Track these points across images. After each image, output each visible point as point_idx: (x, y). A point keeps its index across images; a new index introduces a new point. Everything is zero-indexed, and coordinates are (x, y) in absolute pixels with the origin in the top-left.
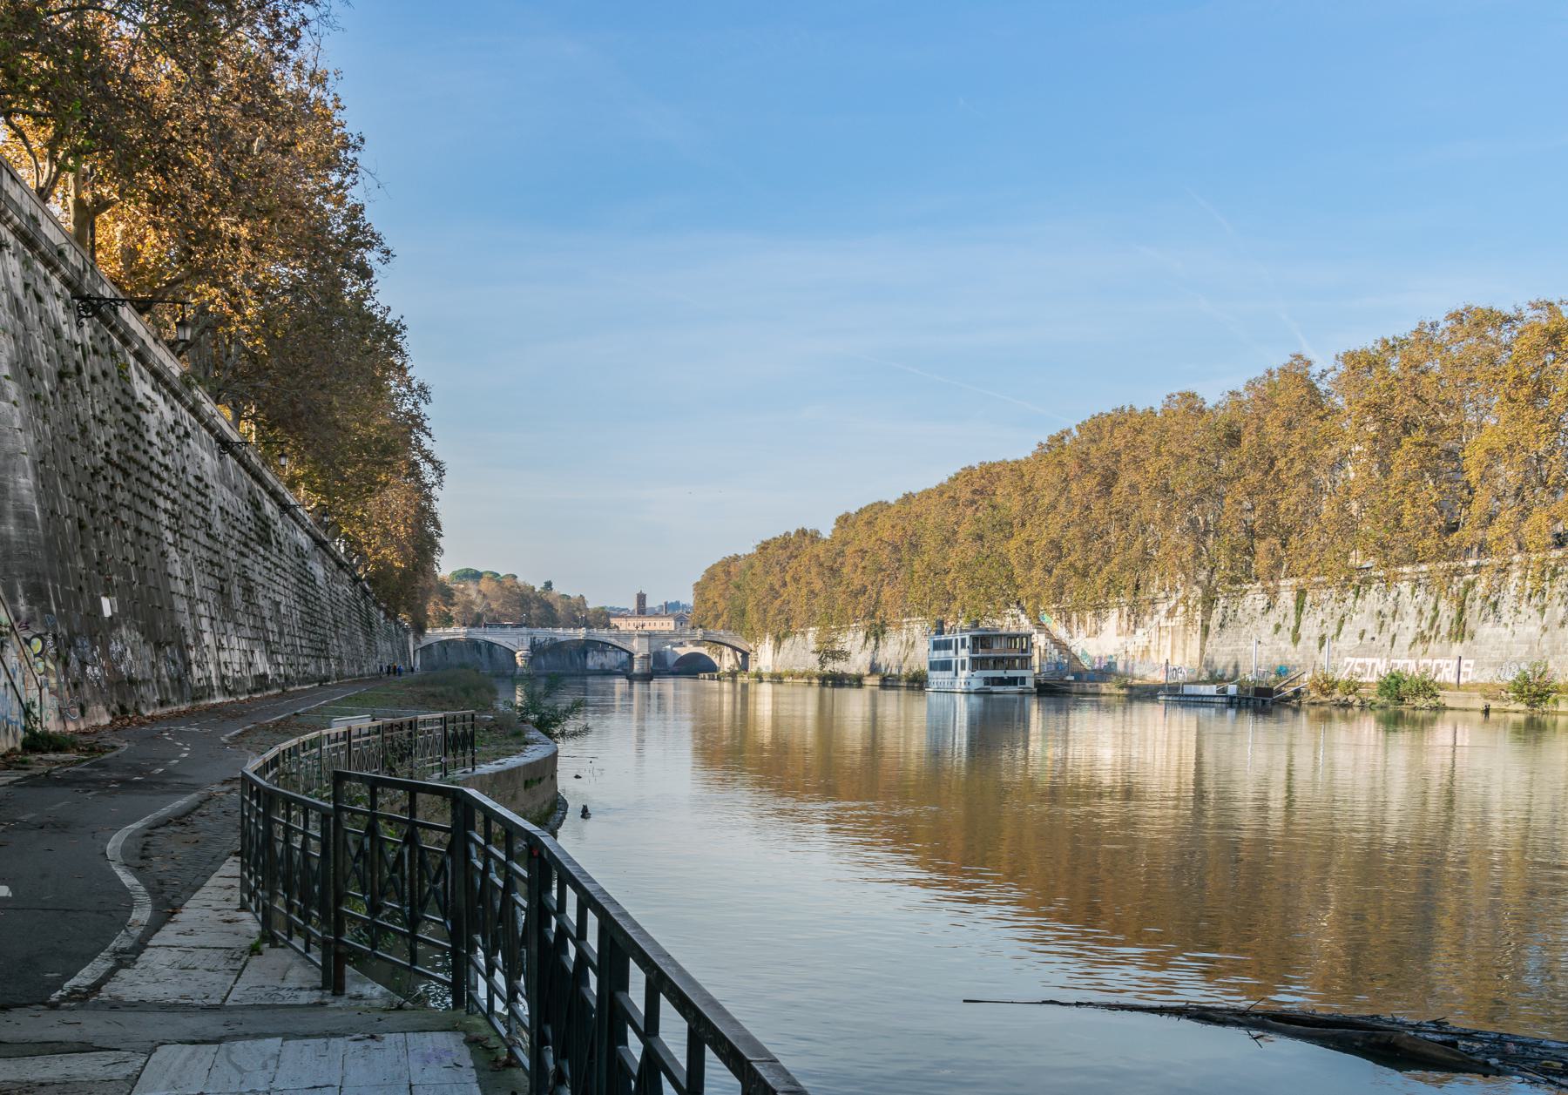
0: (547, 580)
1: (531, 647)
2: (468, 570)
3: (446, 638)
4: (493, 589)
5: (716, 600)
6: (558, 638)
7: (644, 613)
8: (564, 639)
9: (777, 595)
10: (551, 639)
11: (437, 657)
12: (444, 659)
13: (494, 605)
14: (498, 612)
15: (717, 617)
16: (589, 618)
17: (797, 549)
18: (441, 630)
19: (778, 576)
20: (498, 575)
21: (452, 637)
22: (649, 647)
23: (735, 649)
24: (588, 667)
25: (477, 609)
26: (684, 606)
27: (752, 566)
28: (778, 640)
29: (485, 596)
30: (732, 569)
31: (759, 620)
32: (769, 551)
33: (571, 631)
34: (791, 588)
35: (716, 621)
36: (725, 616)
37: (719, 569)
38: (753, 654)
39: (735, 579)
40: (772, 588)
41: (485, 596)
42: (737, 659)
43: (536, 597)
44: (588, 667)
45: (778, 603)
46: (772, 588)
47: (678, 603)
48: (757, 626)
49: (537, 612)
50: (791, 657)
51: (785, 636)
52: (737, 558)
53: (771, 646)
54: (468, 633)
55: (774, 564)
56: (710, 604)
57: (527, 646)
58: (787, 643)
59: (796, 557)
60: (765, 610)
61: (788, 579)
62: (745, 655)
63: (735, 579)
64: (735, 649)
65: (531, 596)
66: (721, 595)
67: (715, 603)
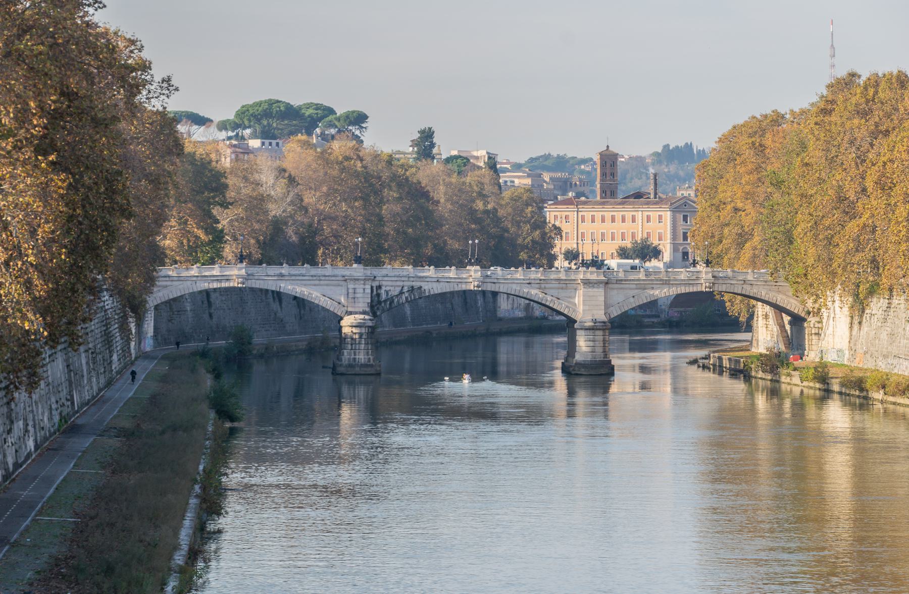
0: (424, 126)
1: (371, 306)
2: (271, 103)
3: (205, 286)
4: (308, 166)
5: (740, 205)
6: (426, 286)
7: (613, 194)
8: (437, 289)
9: (851, 213)
10: (412, 290)
11: (190, 314)
12: (206, 316)
13: (309, 199)
14: (319, 213)
15: (742, 239)
16: (501, 213)
17: (888, 116)
18: (194, 271)
19: (853, 171)
20: (331, 111)
21: (215, 285)
22: (607, 306)
23: (779, 309)
24: (500, 314)
25: (275, 210)
26: (701, 154)
27: (803, 146)
28: (859, 307)
29: (292, 180)
30: (768, 141)
31: (819, 259)
32: (833, 118)
33: (451, 273)
34: (876, 202)
35: (741, 245)
36: (756, 239)
37: (743, 142)
38: (812, 320)
39: (774, 166)
40: (841, 199)
41: (292, 180)
42: (782, 326)
43: (394, 177)
44: (500, 314)
45: (853, 227)
46: (841, 199)
47: (689, 147)
48: (817, 273)
49: (397, 208)
50: (884, 336)
51: (871, 292)
52: (777, 119)
53: (846, 310)
54: (249, 277)
55: (845, 145)
56: (726, 213)
57: (363, 302)
58: (877, 305)
59: (887, 133)
60: (829, 240)
61: (869, 184)
62: (798, 321)
63: (774, 166)
64: (779, 309)
65: (385, 175)
66: (748, 196)
67: (736, 210)
